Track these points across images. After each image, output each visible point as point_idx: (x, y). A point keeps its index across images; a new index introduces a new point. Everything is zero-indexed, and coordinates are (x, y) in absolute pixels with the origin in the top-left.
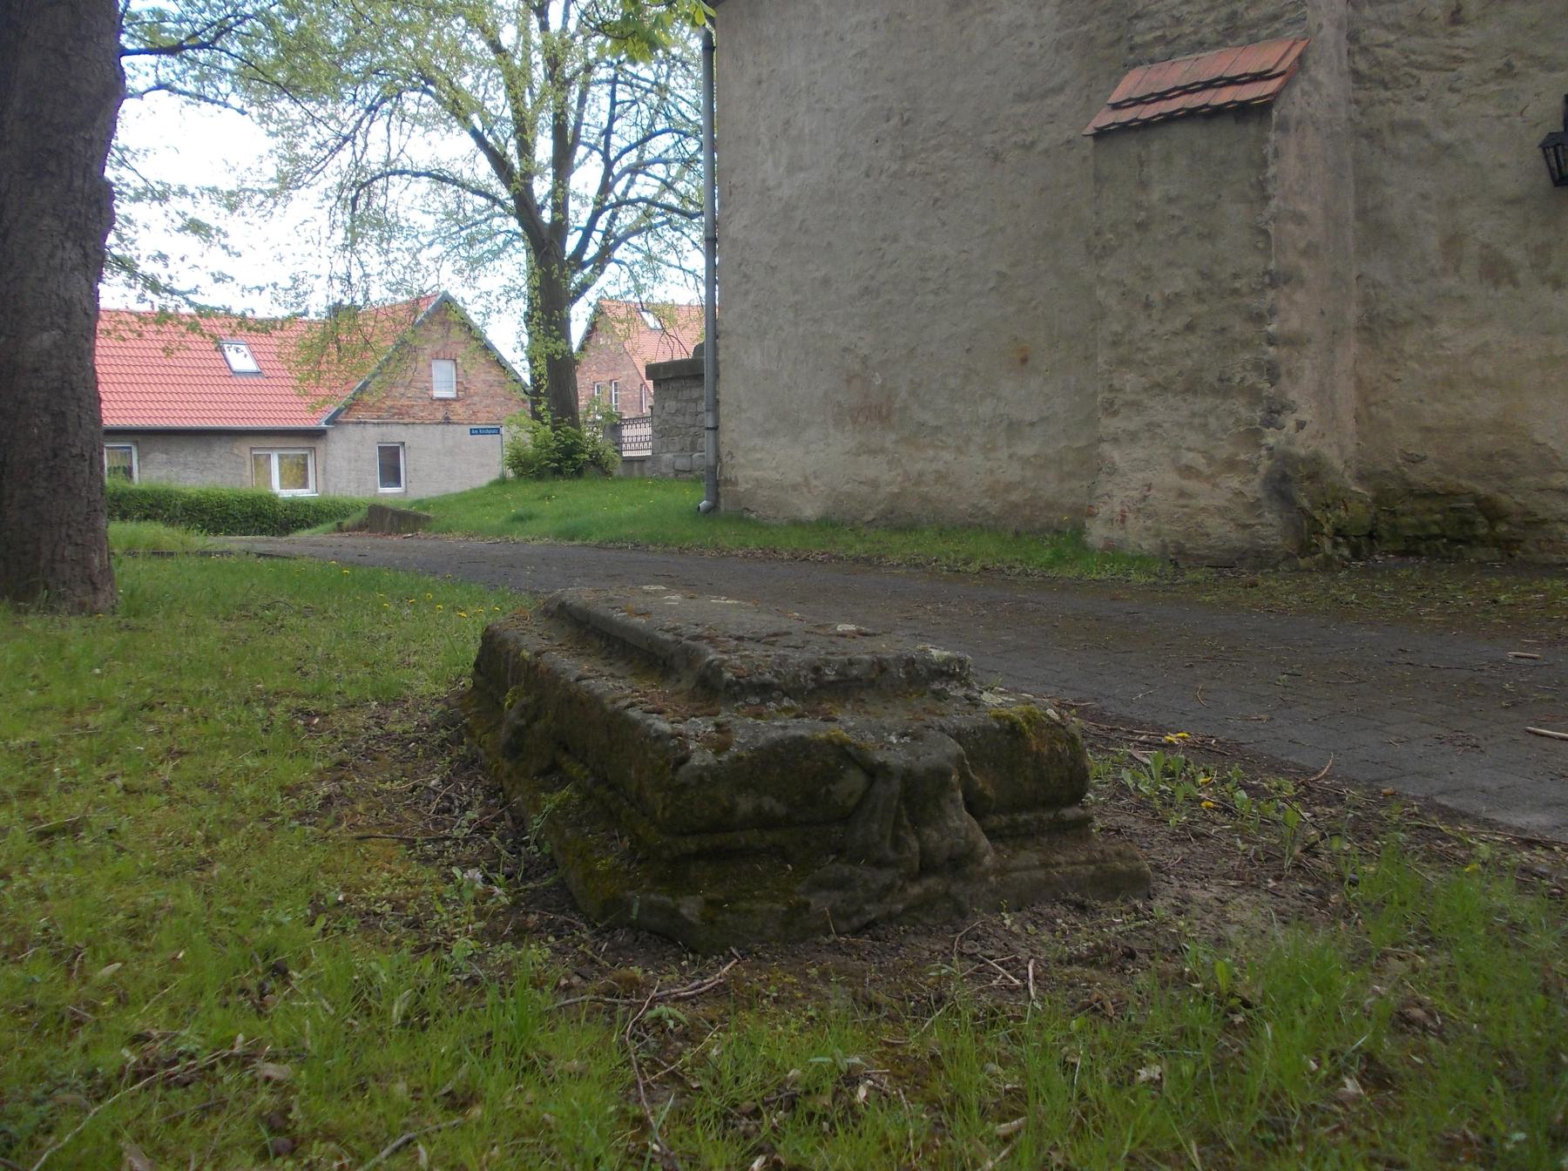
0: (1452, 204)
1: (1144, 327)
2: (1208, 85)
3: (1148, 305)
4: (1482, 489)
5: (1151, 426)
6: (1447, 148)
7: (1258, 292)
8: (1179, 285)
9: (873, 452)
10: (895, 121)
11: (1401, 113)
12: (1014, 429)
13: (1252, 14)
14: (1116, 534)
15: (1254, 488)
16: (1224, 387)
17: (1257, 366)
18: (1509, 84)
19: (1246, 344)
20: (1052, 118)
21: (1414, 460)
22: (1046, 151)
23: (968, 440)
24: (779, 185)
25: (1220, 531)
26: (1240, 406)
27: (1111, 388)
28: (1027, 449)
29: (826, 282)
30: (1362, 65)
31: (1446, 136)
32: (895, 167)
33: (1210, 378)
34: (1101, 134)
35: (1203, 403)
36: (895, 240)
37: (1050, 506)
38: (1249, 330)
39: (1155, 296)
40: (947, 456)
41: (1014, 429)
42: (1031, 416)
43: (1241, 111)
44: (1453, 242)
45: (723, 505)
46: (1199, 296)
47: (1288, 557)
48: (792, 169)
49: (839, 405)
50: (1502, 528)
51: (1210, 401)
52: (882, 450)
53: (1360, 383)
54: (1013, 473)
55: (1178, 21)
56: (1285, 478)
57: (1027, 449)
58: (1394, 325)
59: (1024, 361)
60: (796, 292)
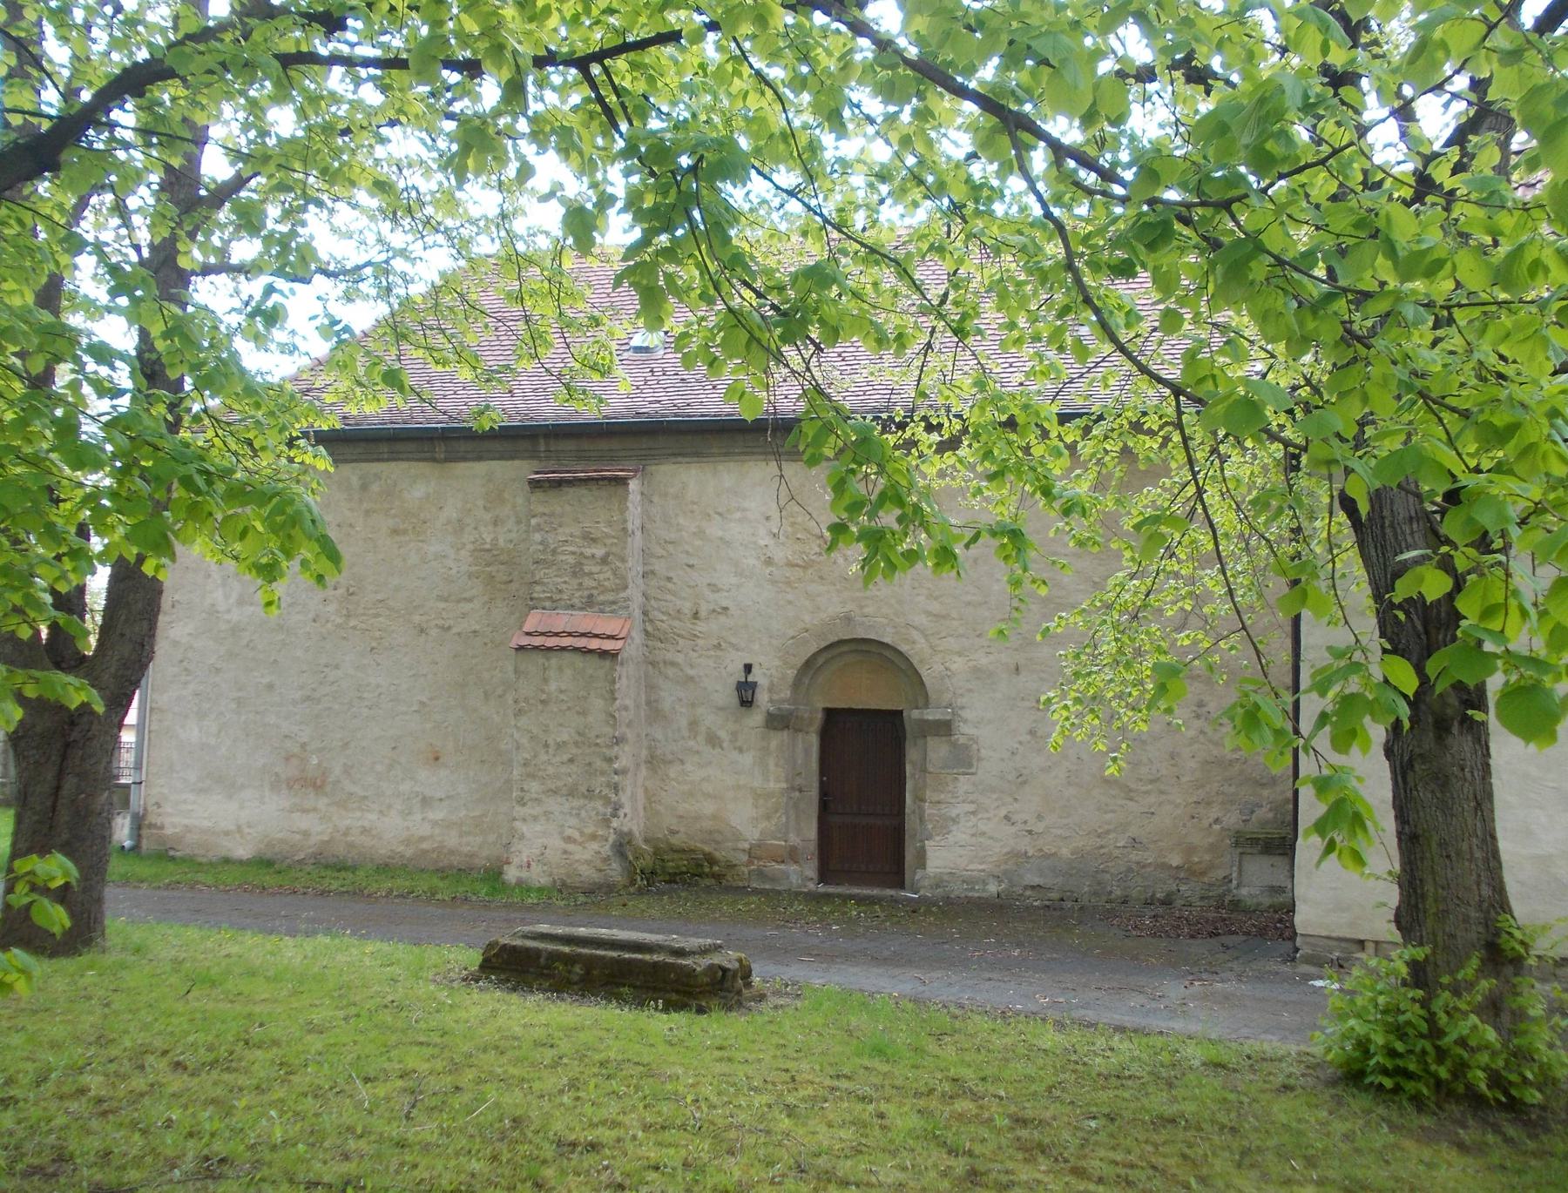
0: (693, 705)
1: (543, 757)
2: (583, 635)
3: (546, 745)
4: (707, 849)
5: (546, 813)
6: (691, 679)
7: (610, 747)
8: (565, 737)
9: (305, 811)
10: (341, 591)
11: (669, 656)
12: (426, 802)
13: (602, 598)
14: (524, 874)
15: (606, 850)
16: (590, 794)
17: (608, 785)
18: (719, 653)
19: (603, 773)
20: (464, 616)
21: (673, 832)
22: (459, 634)
23: (390, 806)
24: (229, 611)
25: (588, 873)
26: (599, 804)
27: (522, 790)
28: (438, 814)
29: (270, 687)
30: (649, 629)
31: (691, 672)
32: (339, 620)
33: (583, 789)
34: (521, 648)
35: (576, 803)
36: (337, 667)
37: (452, 852)
38: (605, 766)
39: (550, 742)
40: (373, 817)
41: (426, 802)
42: (441, 795)
43: (604, 654)
44: (693, 724)
45: (145, 844)
46: (576, 744)
47: (625, 887)
48: (241, 602)
49: (277, 774)
50: (716, 868)
51: (582, 801)
52: (315, 809)
53: (646, 790)
54: (425, 830)
55: (560, 591)
56: (621, 845)
57: (438, 814)
58: (665, 762)
59: (437, 759)
60: (240, 690)
